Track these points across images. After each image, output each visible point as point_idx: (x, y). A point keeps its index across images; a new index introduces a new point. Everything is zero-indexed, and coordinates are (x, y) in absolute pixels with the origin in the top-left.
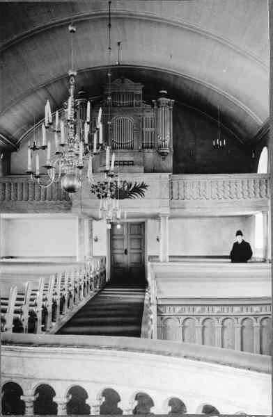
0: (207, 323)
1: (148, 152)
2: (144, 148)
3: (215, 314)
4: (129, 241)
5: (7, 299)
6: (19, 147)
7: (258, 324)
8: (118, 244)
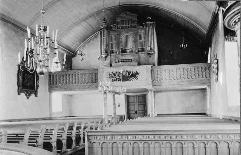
0: (114, 145)
1: (142, 54)
2: (139, 51)
3: (118, 140)
4: (138, 106)
5: (24, 134)
6: (76, 55)
7: (142, 146)
8: (132, 108)
